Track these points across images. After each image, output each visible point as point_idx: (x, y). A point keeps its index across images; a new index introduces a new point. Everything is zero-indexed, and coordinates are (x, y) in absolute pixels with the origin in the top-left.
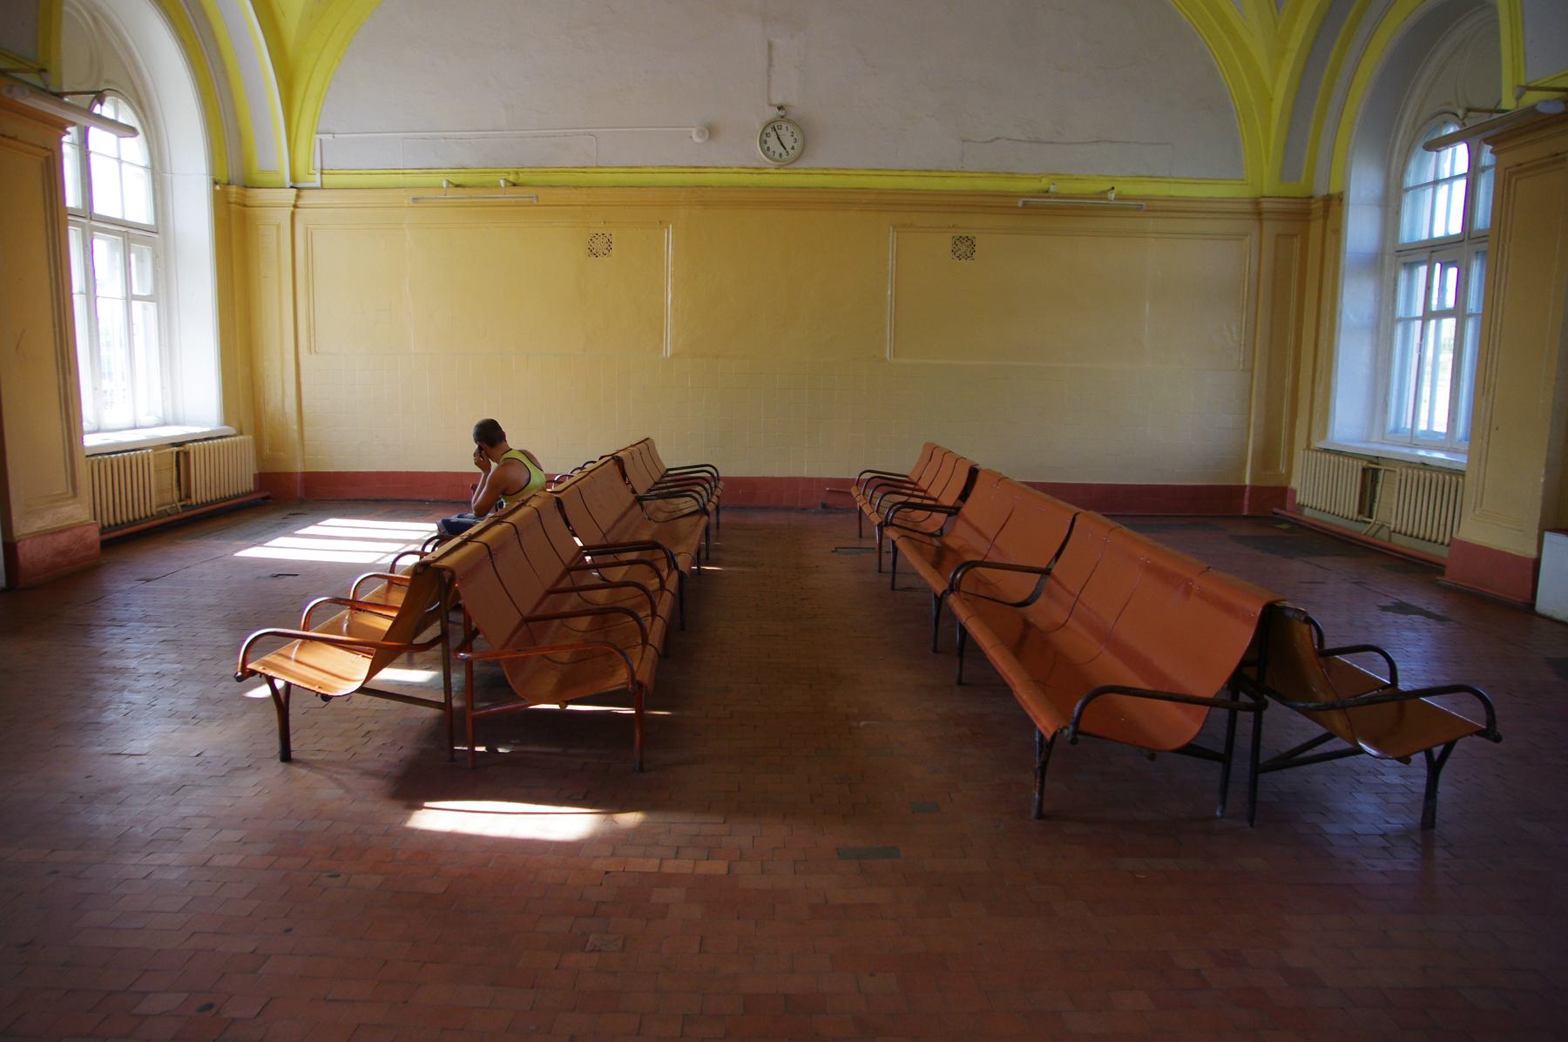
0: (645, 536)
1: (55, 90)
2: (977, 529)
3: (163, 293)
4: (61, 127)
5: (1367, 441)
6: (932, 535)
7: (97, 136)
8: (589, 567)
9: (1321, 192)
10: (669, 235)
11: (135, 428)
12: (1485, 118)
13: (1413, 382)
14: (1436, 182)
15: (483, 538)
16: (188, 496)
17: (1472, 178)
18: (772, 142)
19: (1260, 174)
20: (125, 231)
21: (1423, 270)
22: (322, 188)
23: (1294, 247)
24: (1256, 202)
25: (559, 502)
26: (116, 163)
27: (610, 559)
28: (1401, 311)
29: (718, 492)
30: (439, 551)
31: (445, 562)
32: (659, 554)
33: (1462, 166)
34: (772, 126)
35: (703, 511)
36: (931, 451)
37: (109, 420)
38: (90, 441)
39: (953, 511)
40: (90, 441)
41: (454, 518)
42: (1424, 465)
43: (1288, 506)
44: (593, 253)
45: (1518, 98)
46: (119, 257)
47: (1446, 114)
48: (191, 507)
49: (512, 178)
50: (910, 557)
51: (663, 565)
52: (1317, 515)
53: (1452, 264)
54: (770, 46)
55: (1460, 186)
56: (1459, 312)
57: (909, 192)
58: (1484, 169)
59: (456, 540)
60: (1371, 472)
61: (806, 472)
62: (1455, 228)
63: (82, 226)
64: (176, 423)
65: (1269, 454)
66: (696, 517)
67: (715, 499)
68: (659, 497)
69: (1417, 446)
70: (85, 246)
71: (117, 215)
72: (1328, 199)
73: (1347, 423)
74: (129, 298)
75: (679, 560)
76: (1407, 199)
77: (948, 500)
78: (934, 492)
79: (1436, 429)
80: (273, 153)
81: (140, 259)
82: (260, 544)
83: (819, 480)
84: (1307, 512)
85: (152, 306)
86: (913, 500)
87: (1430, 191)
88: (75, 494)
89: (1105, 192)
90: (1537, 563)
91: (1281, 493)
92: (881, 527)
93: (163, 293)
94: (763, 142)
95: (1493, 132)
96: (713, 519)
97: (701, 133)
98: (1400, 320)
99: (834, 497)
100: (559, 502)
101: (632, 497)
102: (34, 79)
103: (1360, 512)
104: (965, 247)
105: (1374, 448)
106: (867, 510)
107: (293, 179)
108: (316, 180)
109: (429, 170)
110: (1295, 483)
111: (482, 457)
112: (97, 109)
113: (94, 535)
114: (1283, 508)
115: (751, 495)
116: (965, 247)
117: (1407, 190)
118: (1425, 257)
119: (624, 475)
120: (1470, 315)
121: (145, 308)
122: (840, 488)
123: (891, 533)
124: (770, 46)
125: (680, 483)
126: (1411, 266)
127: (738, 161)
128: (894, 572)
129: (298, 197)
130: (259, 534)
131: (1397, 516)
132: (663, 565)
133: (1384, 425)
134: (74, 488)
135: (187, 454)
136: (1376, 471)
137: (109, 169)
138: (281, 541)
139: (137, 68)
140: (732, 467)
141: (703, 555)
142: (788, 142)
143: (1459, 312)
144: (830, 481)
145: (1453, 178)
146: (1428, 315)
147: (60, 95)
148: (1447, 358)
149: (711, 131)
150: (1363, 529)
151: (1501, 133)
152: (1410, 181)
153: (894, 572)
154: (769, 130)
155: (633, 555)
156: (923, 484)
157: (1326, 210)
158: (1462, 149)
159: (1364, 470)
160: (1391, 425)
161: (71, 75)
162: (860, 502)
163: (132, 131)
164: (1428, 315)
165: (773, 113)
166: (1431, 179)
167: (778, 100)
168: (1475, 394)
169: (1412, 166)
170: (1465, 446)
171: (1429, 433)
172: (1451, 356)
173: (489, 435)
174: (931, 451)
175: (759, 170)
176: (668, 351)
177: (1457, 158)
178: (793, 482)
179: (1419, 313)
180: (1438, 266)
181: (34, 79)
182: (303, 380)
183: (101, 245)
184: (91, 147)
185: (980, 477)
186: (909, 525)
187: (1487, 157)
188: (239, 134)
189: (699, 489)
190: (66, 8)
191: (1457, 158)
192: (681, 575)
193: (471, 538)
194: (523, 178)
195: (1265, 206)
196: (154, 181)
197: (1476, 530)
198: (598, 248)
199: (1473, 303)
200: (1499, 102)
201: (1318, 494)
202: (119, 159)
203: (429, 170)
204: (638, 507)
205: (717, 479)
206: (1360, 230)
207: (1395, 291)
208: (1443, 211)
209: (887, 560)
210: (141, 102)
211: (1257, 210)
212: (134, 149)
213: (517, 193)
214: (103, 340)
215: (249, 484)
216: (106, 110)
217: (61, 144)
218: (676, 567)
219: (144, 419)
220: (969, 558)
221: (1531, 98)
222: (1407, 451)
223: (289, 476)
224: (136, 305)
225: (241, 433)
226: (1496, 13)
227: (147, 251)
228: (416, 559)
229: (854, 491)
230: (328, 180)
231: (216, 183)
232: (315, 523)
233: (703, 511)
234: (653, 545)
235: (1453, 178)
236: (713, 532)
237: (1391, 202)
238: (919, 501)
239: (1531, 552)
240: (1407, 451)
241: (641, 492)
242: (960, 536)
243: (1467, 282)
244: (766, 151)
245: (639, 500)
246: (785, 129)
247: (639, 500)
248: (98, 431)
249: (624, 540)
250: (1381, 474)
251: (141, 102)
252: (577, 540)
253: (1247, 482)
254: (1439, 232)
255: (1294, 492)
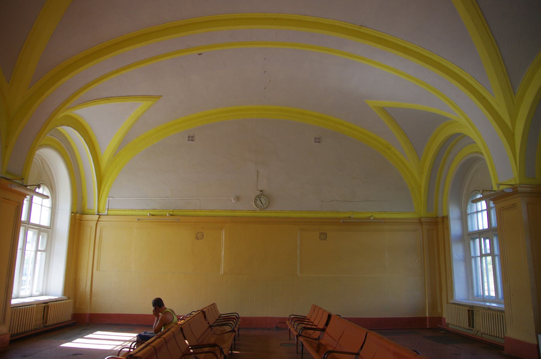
0: (212, 341)
1: (25, 184)
2: (332, 337)
3: (49, 250)
4: (25, 196)
5: (468, 300)
6: (316, 339)
7: (36, 199)
8: (192, 353)
9: (440, 216)
10: (223, 233)
11: (31, 296)
12: (488, 193)
13: (482, 279)
14: (477, 212)
15: (153, 344)
16: (46, 322)
17: (488, 210)
18: (258, 202)
19: (419, 209)
20: (39, 228)
21: (478, 240)
22: (107, 215)
23: (435, 240)
24: (420, 219)
25: (181, 329)
26: (40, 206)
27: (199, 350)
28: (473, 254)
29: (239, 323)
30: (136, 351)
31: (138, 354)
32: (217, 348)
33: (485, 207)
34: (258, 197)
35: (233, 331)
36: (314, 308)
37: (22, 293)
38: (14, 302)
39: (323, 330)
40: (14, 302)
41: (143, 333)
42: (490, 309)
43: (443, 324)
44: (197, 238)
45: (498, 187)
46: (36, 237)
47: (477, 191)
48: (47, 326)
49: (171, 213)
50: (308, 348)
51: (218, 352)
52: (454, 327)
53: (487, 238)
54: (258, 171)
55: (485, 213)
56: (492, 254)
57: (305, 218)
58: (492, 208)
59: (143, 345)
60: (471, 311)
61: (270, 315)
62: (486, 227)
63: (25, 227)
64: (46, 295)
65: (434, 305)
66: (231, 333)
67: (237, 326)
68: (217, 325)
69: (486, 301)
70: (25, 233)
71: (38, 223)
72: (443, 218)
73: (460, 293)
74: (37, 250)
75: (224, 350)
76: (469, 217)
77: (321, 326)
78: (316, 323)
79: (491, 295)
80: (93, 203)
81: (43, 238)
82: (70, 341)
83: (275, 318)
84: (450, 326)
85: (44, 254)
86: (308, 326)
87: (476, 215)
88: (4, 322)
89: (369, 217)
90: (538, 346)
91: (440, 319)
92: (297, 336)
93: (49, 250)
94: (255, 202)
95: (493, 197)
96: (237, 333)
97: (235, 199)
98: (473, 257)
99: (280, 324)
100: (181, 329)
101: (208, 325)
102: (19, 182)
103: (469, 326)
104: (323, 236)
105: (471, 302)
106: (292, 330)
107: (98, 212)
108: (106, 213)
109: (143, 210)
110: (444, 316)
111: (156, 312)
112: (37, 190)
113: (8, 338)
114: (441, 325)
115: (251, 323)
116: (323, 236)
117: (468, 214)
118: (478, 236)
119: (205, 317)
120: (496, 255)
121: (42, 254)
122: (282, 321)
123: (301, 339)
124: (258, 171)
125: (226, 320)
126: (474, 239)
127: (247, 208)
128: (302, 353)
129: (99, 218)
130: (70, 339)
131: (482, 327)
132: (218, 352)
133: (473, 294)
134: (4, 320)
135: (48, 307)
136: (473, 311)
137: (38, 209)
138: (78, 340)
139: (53, 180)
140: (244, 313)
141: (233, 347)
142: (264, 202)
143: (492, 254)
144: (279, 318)
145: (482, 211)
146: (482, 256)
147: (26, 186)
148: (490, 267)
149: (238, 198)
150: (472, 332)
151: (495, 198)
152: (469, 211)
153: (302, 353)
154: (257, 198)
155: (207, 349)
156: (312, 320)
157: (443, 221)
158: (484, 203)
159: (468, 311)
160: (475, 294)
161: (31, 179)
162: (290, 327)
163: (47, 197)
164: (482, 256)
165: (258, 193)
166: (475, 211)
167: (260, 188)
168: (501, 265)
169: (469, 207)
170: (503, 301)
171: (489, 296)
172: (492, 266)
173: (158, 303)
174: (314, 308)
175: (254, 211)
176: (222, 272)
177: (483, 205)
178: (265, 319)
179: (479, 255)
180: (482, 239)
181: (19, 182)
182: (94, 280)
183: (30, 233)
184: (33, 201)
185: (332, 318)
186: (307, 336)
187: (492, 204)
188: (82, 197)
189: (231, 322)
190: (34, 160)
191: (483, 205)
192: (225, 356)
193: (148, 344)
194: (175, 213)
195: (423, 220)
196: (52, 212)
197: (511, 334)
198: (199, 237)
199: (496, 251)
200: (492, 188)
201: (453, 320)
202: (42, 205)
203: (143, 210)
204: (210, 329)
205: (238, 318)
206: (455, 228)
207: (470, 248)
208: (481, 221)
209: (300, 348)
210: (52, 188)
211: (420, 222)
212: (47, 202)
213: (172, 218)
214: (25, 262)
215: (69, 318)
216: (40, 190)
217: (24, 200)
218: (223, 353)
219: (35, 293)
220: (330, 349)
221: (502, 187)
222: (482, 303)
223: (84, 315)
224: (39, 253)
225: (69, 299)
226: (486, 161)
227: (46, 235)
228: (128, 350)
229: (287, 322)
230: (110, 212)
231: (72, 213)
232: (92, 333)
233: (233, 331)
234: (214, 345)
235: (482, 211)
236: (237, 338)
237: (464, 218)
238: (310, 326)
239: (536, 342)
240: (482, 303)
241: (211, 324)
242: (326, 340)
243: (493, 244)
244: (256, 205)
245: (211, 326)
246: (263, 198)
247: (211, 326)
248: (17, 298)
249: (204, 343)
250: (475, 312)
251: (52, 188)
252: (186, 341)
253: (427, 315)
254: (474, 230)
255: (445, 319)
